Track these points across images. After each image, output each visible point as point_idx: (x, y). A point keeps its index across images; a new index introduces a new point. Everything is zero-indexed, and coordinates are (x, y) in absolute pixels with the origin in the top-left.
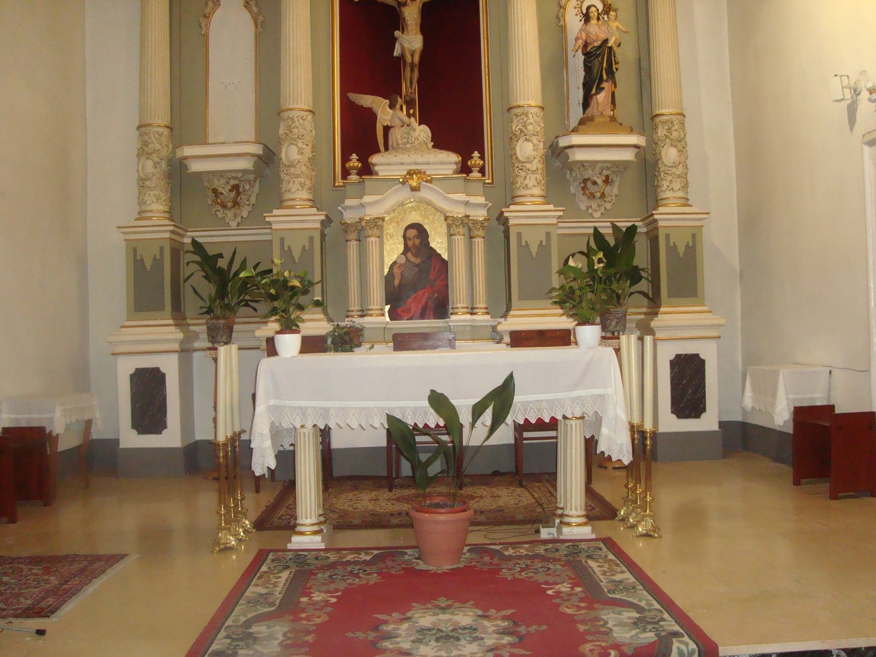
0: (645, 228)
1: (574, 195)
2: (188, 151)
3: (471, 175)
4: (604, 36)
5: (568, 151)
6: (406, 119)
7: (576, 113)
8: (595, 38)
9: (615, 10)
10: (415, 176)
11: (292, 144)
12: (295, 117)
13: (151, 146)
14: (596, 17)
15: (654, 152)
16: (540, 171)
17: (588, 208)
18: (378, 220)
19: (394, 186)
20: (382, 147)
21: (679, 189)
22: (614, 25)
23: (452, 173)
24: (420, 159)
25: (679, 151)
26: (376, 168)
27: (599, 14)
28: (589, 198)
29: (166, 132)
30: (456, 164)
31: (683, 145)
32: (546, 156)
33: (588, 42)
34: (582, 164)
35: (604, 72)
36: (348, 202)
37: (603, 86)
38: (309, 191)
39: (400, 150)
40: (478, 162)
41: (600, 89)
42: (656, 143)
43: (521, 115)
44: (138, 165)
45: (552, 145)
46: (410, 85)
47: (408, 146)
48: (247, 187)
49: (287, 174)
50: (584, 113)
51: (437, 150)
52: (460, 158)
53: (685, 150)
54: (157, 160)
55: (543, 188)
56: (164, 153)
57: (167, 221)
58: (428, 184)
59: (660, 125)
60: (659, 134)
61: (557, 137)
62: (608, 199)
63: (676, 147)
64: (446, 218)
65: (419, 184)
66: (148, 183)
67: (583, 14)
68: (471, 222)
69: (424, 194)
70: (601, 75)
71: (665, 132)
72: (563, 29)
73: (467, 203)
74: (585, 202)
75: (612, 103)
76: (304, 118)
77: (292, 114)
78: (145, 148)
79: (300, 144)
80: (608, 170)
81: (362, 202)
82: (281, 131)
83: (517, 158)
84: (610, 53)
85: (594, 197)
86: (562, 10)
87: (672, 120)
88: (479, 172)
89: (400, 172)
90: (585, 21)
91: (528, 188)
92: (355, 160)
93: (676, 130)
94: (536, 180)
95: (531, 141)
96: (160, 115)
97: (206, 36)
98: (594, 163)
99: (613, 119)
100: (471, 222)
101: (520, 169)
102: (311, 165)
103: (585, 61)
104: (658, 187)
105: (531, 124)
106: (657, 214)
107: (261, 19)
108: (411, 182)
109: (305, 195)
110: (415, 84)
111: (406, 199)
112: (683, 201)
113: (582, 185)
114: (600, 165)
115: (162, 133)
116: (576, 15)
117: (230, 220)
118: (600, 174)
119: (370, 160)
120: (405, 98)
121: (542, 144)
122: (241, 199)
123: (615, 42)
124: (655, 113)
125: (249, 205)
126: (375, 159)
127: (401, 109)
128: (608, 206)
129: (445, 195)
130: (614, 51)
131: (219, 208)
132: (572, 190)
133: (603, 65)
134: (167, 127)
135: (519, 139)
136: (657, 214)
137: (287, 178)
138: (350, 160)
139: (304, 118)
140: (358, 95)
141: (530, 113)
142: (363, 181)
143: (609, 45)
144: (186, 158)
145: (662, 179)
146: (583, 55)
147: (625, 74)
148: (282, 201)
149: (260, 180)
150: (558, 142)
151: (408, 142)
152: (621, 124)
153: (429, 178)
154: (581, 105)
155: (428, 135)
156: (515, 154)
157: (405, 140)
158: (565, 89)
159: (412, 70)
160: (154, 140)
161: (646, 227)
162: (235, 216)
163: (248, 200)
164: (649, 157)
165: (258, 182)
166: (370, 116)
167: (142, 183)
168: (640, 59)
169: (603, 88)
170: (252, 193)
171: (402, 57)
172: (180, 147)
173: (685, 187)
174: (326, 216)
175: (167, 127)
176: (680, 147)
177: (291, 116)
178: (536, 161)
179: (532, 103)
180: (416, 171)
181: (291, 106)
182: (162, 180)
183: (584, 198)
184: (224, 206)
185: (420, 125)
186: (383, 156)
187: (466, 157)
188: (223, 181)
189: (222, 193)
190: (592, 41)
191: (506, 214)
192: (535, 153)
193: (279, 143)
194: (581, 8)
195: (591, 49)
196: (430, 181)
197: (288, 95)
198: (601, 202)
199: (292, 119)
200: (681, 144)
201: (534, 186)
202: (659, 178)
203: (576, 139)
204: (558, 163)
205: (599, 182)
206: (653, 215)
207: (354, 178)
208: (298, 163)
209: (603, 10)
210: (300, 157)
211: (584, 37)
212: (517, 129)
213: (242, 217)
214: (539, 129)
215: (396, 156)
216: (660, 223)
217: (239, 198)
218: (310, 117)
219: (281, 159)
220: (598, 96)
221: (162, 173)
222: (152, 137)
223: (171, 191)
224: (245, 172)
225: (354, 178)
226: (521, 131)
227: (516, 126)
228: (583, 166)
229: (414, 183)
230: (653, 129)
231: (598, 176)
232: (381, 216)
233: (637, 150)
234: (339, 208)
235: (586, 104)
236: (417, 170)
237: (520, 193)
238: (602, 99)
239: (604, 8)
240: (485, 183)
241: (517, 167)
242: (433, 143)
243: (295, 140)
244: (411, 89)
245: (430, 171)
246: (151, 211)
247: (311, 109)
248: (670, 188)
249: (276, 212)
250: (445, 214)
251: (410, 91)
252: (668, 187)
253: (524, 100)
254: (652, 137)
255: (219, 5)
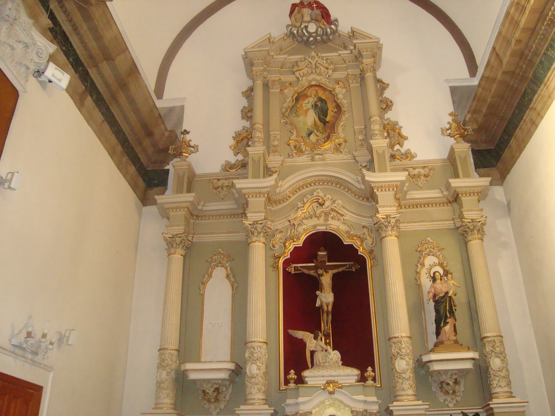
0: (485, 413)
1: (435, 392)
2: (189, 366)
3: (367, 382)
4: (445, 290)
5: (428, 364)
6: (325, 346)
7: (432, 339)
8: (440, 291)
9: (451, 274)
10: (331, 384)
11: (253, 363)
12: (256, 346)
13: (166, 362)
14: (439, 279)
15: (485, 362)
16: (411, 379)
17: (445, 401)
18: (308, 414)
19: (318, 391)
20: (310, 365)
21: (505, 386)
22: (451, 282)
23: (355, 382)
24: (333, 373)
25: (502, 360)
26: (306, 379)
27: (441, 276)
28: (445, 394)
29: (176, 353)
30: (357, 375)
31: (504, 356)
32: (415, 368)
33: (436, 294)
34: (439, 372)
35: (448, 312)
36: (289, 401)
37: (448, 321)
38: (263, 394)
39: (321, 368)
40: (371, 374)
41: (446, 323)
42: (486, 356)
43: (397, 343)
44: (157, 373)
45: (418, 360)
46: (326, 324)
47: (326, 364)
48: (224, 389)
49: (250, 383)
50: (437, 338)
51: (344, 367)
52: (360, 372)
53: (505, 360)
54: (169, 370)
55: (414, 389)
56: (174, 366)
57: (173, 410)
58: (340, 390)
59: (487, 343)
60: (487, 349)
61: (421, 355)
62: (458, 394)
63: (499, 357)
64: (352, 412)
65: (334, 389)
66: (162, 385)
67: (431, 277)
68: (369, 414)
69: (336, 396)
70: (446, 315)
71: (491, 348)
72: (419, 286)
73: (365, 402)
74: (443, 397)
75: (454, 331)
76: (261, 347)
77: (253, 344)
78: (162, 363)
79: (258, 364)
80: (456, 375)
81: (297, 401)
82: (247, 355)
83: (396, 370)
84: (450, 301)
85: (448, 393)
86: (418, 274)
87: (494, 340)
88: (372, 380)
89: (321, 382)
90: (433, 281)
91: (404, 390)
92: (293, 374)
93: (498, 347)
94: (409, 384)
95: (405, 359)
96: (173, 342)
97: (203, 295)
98: (446, 371)
99: (456, 342)
100: (369, 414)
101: (398, 378)
102: (265, 377)
103: (435, 305)
104: (490, 385)
105: (404, 348)
106: (492, 404)
107: (236, 285)
108: (329, 388)
109: (261, 396)
110: (330, 324)
111: (326, 400)
112: (509, 394)
113: (440, 385)
114: (450, 372)
115: (173, 354)
116: (427, 278)
117: (213, 410)
118: (451, 378)
119: (302, 374)
120: (323, 333)
121: (411, 360)
122: (220, 397)
123: (452, 293)
124: (483, 336)
125: (225, 401)
126: (306, 373)
127: (321, 339)
128: (459, 399)
129: (350, 396)
130: (452, 299)
131: (206, 402)
132: (434, 389)
133: (446, 308)
134: (176, 350)
135: (397, 358)
136: (492, 404)
137: (250, 385)
138: (290, 374)
139: (261, 347)
140: (294, 331)
141: (402, 341)
142: (298, 388)
143: (449, 295)
144: (187, 370)
145: (493, 379)
146: (434, 302)
147: (461, 312)
148: (246, 400)
149: (232, 385)
150: (422, 359)
151: (326, 362)
152: (462, 345)
153: (340, 386)
154: (435, 334)
155: (339, 357)
156: (395, 368)
157: (324, 360)
158: (424, 324)
159: (328, 315)
160: (168, 359)
161: (485, 412)
162: (216, 408)
163: (224, 398)
164: (482, 365)
165: (231, 386)
166: (302, 344)
167: (159, 385)
168: (469, 302)
169: (448, 323)
170: (228, 393)
171: (321, 307)
172: (184, 363)
173: (509, 384)
174: (274, 410)
175: (176, 350)
176: (502, 358)
177: (253, 346)
178: (409, 372)
179: (404, 335)
180: (332, 382)
181: (253, 340)
182: (172, 383)
183: (442, 394)
184: (209, 401)
185: (333, 350)
186: (310, 372)
187: (363, 370)
188: (209, 385)
189: (208, 393)
190: (439, 293)
191: (391, 408)
192: (407, 367)
193: (245, 362)
194: (430, 273)
195: (438, 298)
196: (341, 388)
197: (251, 333)
198: (453, 396)
199: (254, 348)
200: (502, 355)
201: (408, 388)
202: (491, 379)
203: (434, 356)
204: (423, 372)
205: (451, 383)
206: (489, 405)
207: (292, 385)
208: (257, 376)
209: (444, 274)
210: (258, 372)
211: (433, 290)
212: (395, 352)
213: (220, 409)
214: (409, 351)
215: (318, 371)
216: (495, 411)
217: (219, 396)
218: (265, 346)
219: (246, 373)
220: (445, 328)
221: (172, 379)
222: (167, 356)
223: (176, 391)
224: (223, 380)
225: (292, 385)
226: (398, 353)
227: (394, 350)
228: (439, 373)
229: (330, 389)
230: (483, 346)
231: (450, 379)
232: (310, 411)
233: (474, 361)
234: (283, 405)
235: (438, 333)
236: (333, 380)
237: (401, 393)
238: (448, 329)
239: (444, 272)
240: (376, 387)
241: (397, 376)
242: (342, 362)
243: (255, 361)
244: (327, 326)
245: (342, 381)
246: (163, 403)
247: (265, 341)
248: (499, 386)
249: (242, 407)
250: (351, 409)
251: (327, 328)
252: (497, 384)
253: (398, 333)
254: (483, 351)
255: (212, 277)
